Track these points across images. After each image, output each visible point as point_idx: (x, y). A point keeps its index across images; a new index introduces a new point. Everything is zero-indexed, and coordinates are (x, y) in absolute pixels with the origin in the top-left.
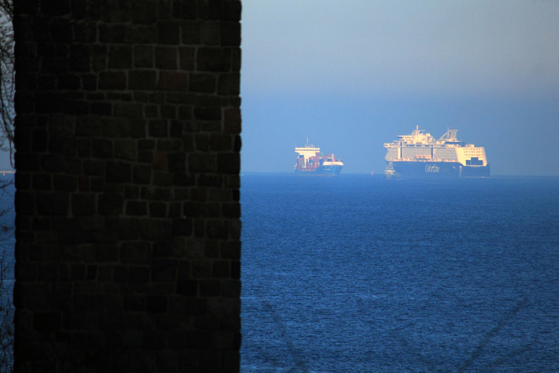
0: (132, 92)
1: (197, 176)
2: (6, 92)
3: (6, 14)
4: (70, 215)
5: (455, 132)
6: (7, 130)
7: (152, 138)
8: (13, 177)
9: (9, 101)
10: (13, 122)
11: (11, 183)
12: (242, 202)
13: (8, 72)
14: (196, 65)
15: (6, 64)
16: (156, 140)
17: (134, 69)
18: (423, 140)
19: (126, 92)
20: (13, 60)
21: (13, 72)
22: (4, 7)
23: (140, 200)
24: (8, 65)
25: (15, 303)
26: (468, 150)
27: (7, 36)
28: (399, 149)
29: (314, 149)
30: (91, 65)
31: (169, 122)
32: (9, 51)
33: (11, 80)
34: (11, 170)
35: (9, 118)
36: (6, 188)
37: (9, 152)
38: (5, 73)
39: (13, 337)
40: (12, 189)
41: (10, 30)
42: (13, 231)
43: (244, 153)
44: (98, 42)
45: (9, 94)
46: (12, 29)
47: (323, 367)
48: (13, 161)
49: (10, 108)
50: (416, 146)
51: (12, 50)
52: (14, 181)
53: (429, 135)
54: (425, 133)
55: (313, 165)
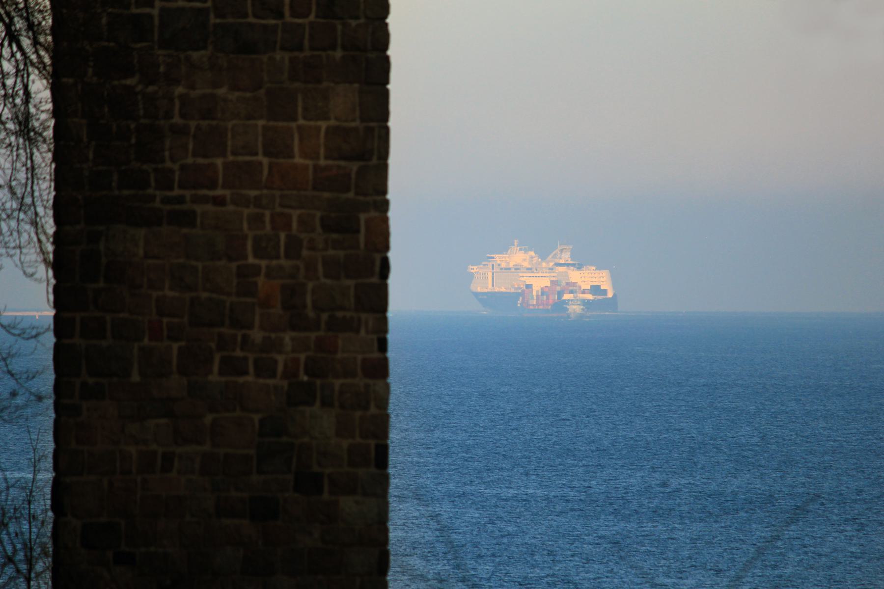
0: (227, 193)
1: (325, 316)
2: (41, 195)
3: (41, 79)
4: (136, 378)
5: (568, 249)
6: (42, 251)
7: (257, 261)
8: (51, 321)
9: (45, 207)
10: (51, 240)
11: (48, 330)
12: (391, 354)
13: (43, 165)
14: (322, 152)
15: (41, 153)
16: (263, 263)
17: (231, 158)
18: (524, 260)
19: (219, 192)
20: (52, 146)
21: (50, 165)
22: (38, 69)
23: (239, 353)
24: (44, 155)
25: (54, 508)
26: (586, 275)
27: (42, 111)
28: (490, 274)
29: (548, 275)
30: (167, 154)
31: (283, 236)
32: (45, 134)
33: (48, 177)
34: (48, 310)
35: (45, 233)
36: (41, 338)
37: (45, 283)
38: (39, 167)
39: (50, 559)
40: (50, 339)
41: (46, 102)
42: (51, 401)
43: (394, 282)
44: (177, 119)
45: (45, 198)
46: (50, 100)
48: (51, 297)
49: (47, 219)
50: (513, 270)
51: (49, 134)
52: (52, 327)
53: (532, 253)
54: (526, 251)
55: (548, 298)
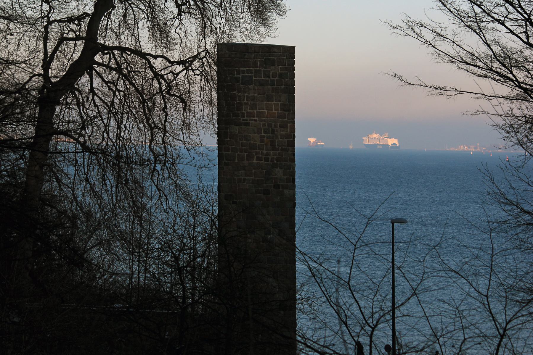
0: (257, 118)
1: (280, 148)
4: (236, 161)
16: (266, 135)
19: (255, 118)
23: (260, 156)
40: (217, 152)
43: (296, 140)
44: (246, 101)
47: (466, 267)
